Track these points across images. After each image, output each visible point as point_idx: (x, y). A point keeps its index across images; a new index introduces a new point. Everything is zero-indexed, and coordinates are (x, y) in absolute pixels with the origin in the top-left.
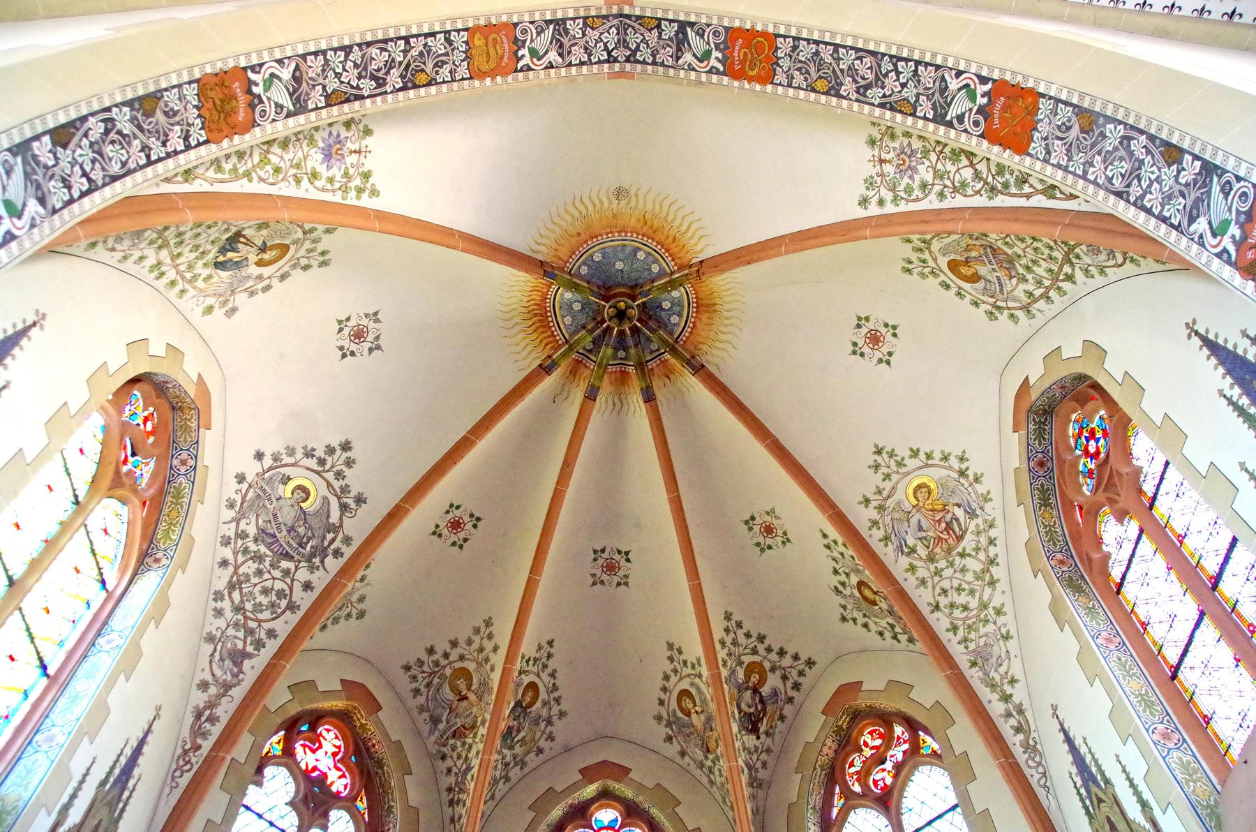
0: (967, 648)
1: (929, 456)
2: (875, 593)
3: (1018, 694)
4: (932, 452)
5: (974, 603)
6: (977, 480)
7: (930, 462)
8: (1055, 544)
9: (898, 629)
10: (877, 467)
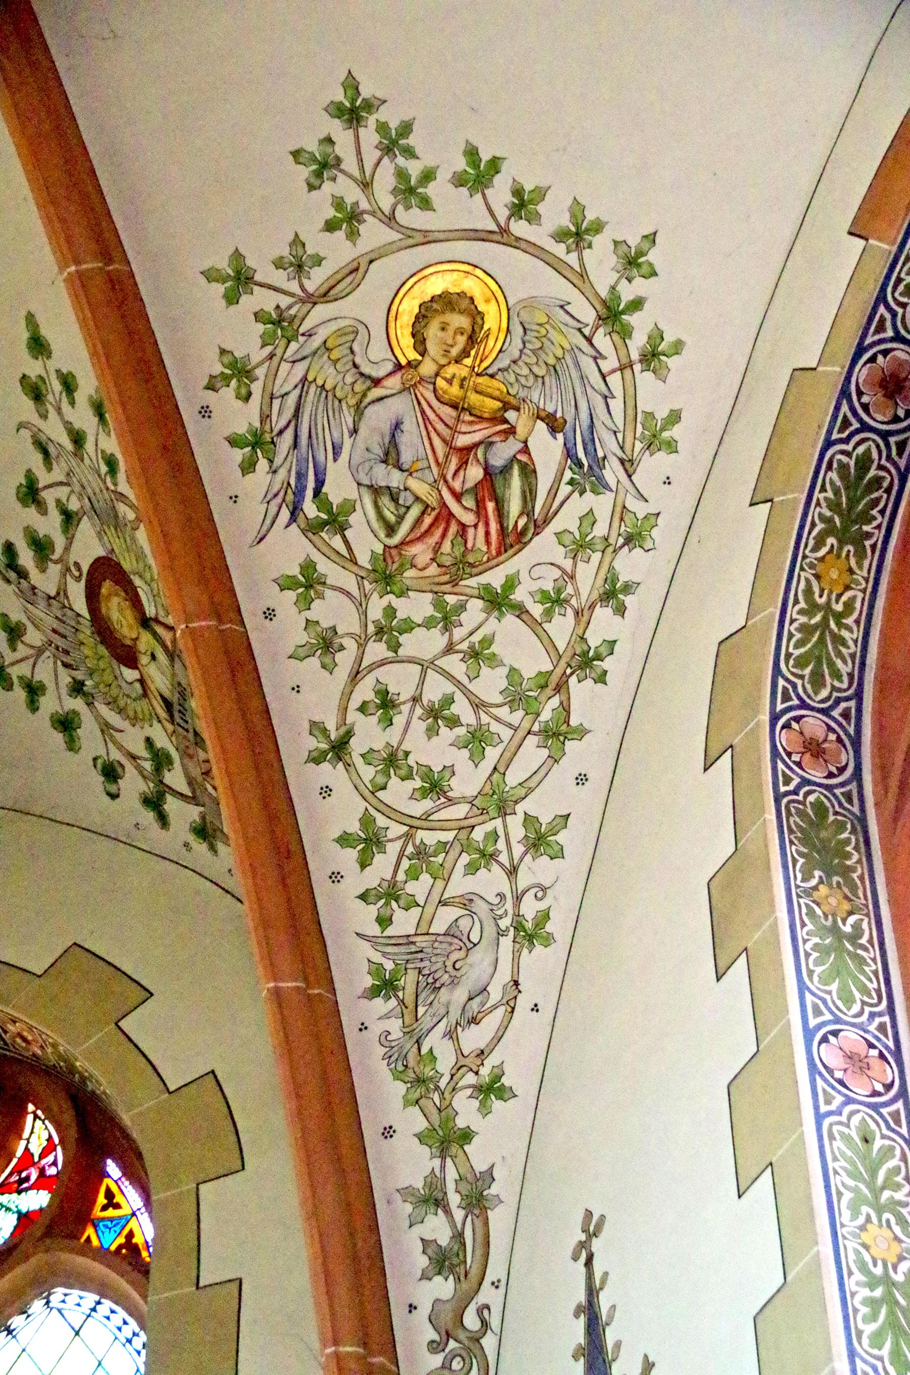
0: (384, 921)
1: (523, 204)
2: (145, 622)
3: (495, 1137)
4: (541, 193)
5: (468, 781)
6: (651, 357)
7: (519, 228)
8: (817, 681)
9: (175, 778)
10: (325, 166)
